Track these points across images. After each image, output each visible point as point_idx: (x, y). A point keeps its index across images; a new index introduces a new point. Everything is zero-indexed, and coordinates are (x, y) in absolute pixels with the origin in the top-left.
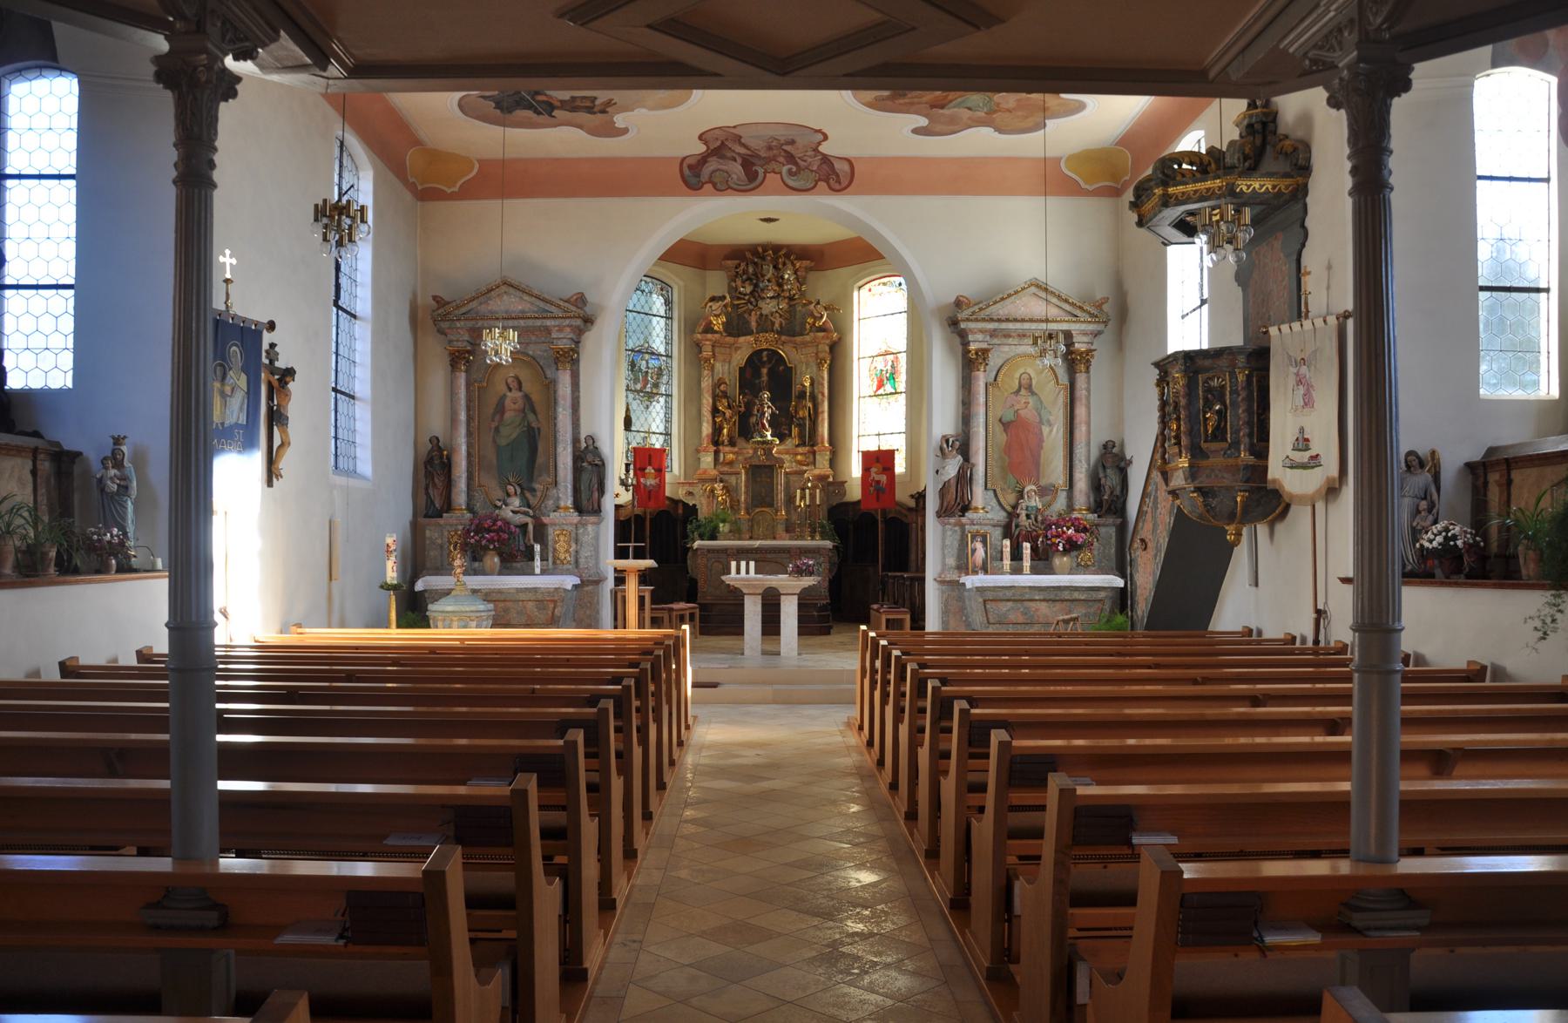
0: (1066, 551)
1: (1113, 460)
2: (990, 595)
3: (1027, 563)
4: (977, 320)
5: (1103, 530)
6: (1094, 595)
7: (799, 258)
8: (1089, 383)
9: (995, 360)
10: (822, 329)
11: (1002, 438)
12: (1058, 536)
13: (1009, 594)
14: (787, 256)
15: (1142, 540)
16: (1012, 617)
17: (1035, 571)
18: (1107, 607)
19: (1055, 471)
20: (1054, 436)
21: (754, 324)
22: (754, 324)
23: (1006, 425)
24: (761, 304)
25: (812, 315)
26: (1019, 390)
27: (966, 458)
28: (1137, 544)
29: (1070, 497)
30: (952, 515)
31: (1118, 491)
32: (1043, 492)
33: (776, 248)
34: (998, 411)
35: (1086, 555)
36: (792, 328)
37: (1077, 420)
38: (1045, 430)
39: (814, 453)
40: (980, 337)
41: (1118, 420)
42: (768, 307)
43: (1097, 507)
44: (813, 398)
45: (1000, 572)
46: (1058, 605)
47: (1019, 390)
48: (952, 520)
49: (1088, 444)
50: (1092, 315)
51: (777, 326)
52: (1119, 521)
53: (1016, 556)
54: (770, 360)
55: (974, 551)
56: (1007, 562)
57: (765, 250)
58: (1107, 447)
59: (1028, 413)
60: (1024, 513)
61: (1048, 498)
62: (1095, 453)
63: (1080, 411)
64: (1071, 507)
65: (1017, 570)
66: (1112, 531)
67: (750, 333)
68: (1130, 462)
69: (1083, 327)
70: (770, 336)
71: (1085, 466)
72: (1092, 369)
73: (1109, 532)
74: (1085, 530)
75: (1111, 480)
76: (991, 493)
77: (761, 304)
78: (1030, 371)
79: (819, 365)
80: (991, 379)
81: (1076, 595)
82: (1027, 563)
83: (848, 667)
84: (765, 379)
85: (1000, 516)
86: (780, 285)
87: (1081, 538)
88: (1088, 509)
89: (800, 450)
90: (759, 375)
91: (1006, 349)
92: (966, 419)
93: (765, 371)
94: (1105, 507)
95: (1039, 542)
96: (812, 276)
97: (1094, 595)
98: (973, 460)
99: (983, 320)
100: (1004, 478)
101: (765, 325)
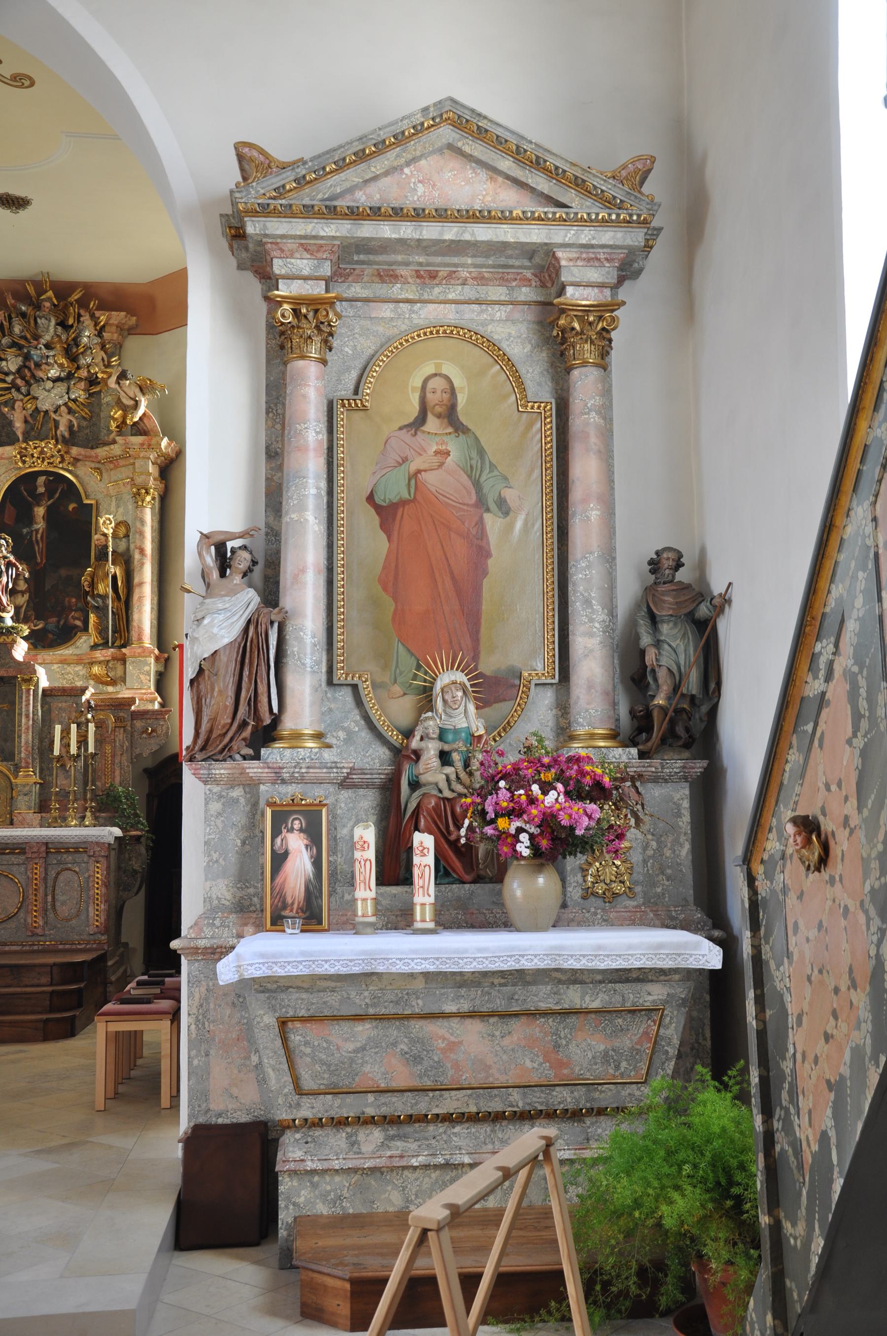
0: (541, 857)
1: (681, 603)
2: (297, 1004)
3: (425, 892)
4: (288, 212)
5: (653, 793)
6: (632, 996)
7: (104, 306)
8: (607, 393)
9: (355, 337)
10: (139, 429)
11: (370, 543)
12: (515, 812)
13: (360, 1000)
14: (83, 303)
15: (808, 826)
16: (374, 1071)
17: (451, 918)
18: (673, 1032)
19: (518, 639)
20: (515, 538)
21: (19, 426)
22: (19, 426)
23: (387, 514)
24: (37, 391)
25: (119, 404)
26: (421, 419)
27: (271, 594)
28: (784, 838)
29: (563, 707)
30: (225, 753)
31: (693, 683)
32: (491, 690)
33: (63, 290)
34: (356, 479)
35: (606, 868)
36: (87, 434)
37: (576, 494)
38: (493, 523)
39: (123, 660)
40: (303, 264)
41: (684, 485)
42: (50, 397)
43: (640, 730)
44: (126, 561)
45: (347, 923)
46: (519, 1029)
47: (421, 419)
48: (221, 770)
49: (609, 557)
50: (609, 203)
51: (63, 428)
52: (699, 766)
53: (394, 868)
54: (50, 492)
55: (280, 859)
56: (366, 892)
57: (40, 291)
58: (662, 566)
59: (446, 481)
60: (431, 750)
61: (502, 709)
62: (629, 588)
63: (585, 469)
64: (565, 732)
65: (399, 919)
66: (681, 794)
67: (11, 440)
68: (726, 601)
69: (586, 236)
70: (49, 447)
71: (601, 615)
72: (615, 356)
73: (668, 796)
74: (598, 792)
75: (673, 652)
76: (345, 696)
77: (37, 391)
78: (448, 369)
79: (137, 497)
80: (346, 388)
81: (574, 997)
82: (425, 892)
83: (163, 1100)
84: (40, 525)
85: (375, 759)
86: (73, 358)
87: (584, 816)
88: (613, 736)
89: (99, 655)
90: (30, 519)
91: (386, 311)
92: (274, 496)
93: (40, 511)
94: (658, 729)
95: (463, 839)
96: (133, 344)
97: (632, 996)
98: (287, 601)
99: (308, 212)
100: (383, 657)
101: (39, 425)
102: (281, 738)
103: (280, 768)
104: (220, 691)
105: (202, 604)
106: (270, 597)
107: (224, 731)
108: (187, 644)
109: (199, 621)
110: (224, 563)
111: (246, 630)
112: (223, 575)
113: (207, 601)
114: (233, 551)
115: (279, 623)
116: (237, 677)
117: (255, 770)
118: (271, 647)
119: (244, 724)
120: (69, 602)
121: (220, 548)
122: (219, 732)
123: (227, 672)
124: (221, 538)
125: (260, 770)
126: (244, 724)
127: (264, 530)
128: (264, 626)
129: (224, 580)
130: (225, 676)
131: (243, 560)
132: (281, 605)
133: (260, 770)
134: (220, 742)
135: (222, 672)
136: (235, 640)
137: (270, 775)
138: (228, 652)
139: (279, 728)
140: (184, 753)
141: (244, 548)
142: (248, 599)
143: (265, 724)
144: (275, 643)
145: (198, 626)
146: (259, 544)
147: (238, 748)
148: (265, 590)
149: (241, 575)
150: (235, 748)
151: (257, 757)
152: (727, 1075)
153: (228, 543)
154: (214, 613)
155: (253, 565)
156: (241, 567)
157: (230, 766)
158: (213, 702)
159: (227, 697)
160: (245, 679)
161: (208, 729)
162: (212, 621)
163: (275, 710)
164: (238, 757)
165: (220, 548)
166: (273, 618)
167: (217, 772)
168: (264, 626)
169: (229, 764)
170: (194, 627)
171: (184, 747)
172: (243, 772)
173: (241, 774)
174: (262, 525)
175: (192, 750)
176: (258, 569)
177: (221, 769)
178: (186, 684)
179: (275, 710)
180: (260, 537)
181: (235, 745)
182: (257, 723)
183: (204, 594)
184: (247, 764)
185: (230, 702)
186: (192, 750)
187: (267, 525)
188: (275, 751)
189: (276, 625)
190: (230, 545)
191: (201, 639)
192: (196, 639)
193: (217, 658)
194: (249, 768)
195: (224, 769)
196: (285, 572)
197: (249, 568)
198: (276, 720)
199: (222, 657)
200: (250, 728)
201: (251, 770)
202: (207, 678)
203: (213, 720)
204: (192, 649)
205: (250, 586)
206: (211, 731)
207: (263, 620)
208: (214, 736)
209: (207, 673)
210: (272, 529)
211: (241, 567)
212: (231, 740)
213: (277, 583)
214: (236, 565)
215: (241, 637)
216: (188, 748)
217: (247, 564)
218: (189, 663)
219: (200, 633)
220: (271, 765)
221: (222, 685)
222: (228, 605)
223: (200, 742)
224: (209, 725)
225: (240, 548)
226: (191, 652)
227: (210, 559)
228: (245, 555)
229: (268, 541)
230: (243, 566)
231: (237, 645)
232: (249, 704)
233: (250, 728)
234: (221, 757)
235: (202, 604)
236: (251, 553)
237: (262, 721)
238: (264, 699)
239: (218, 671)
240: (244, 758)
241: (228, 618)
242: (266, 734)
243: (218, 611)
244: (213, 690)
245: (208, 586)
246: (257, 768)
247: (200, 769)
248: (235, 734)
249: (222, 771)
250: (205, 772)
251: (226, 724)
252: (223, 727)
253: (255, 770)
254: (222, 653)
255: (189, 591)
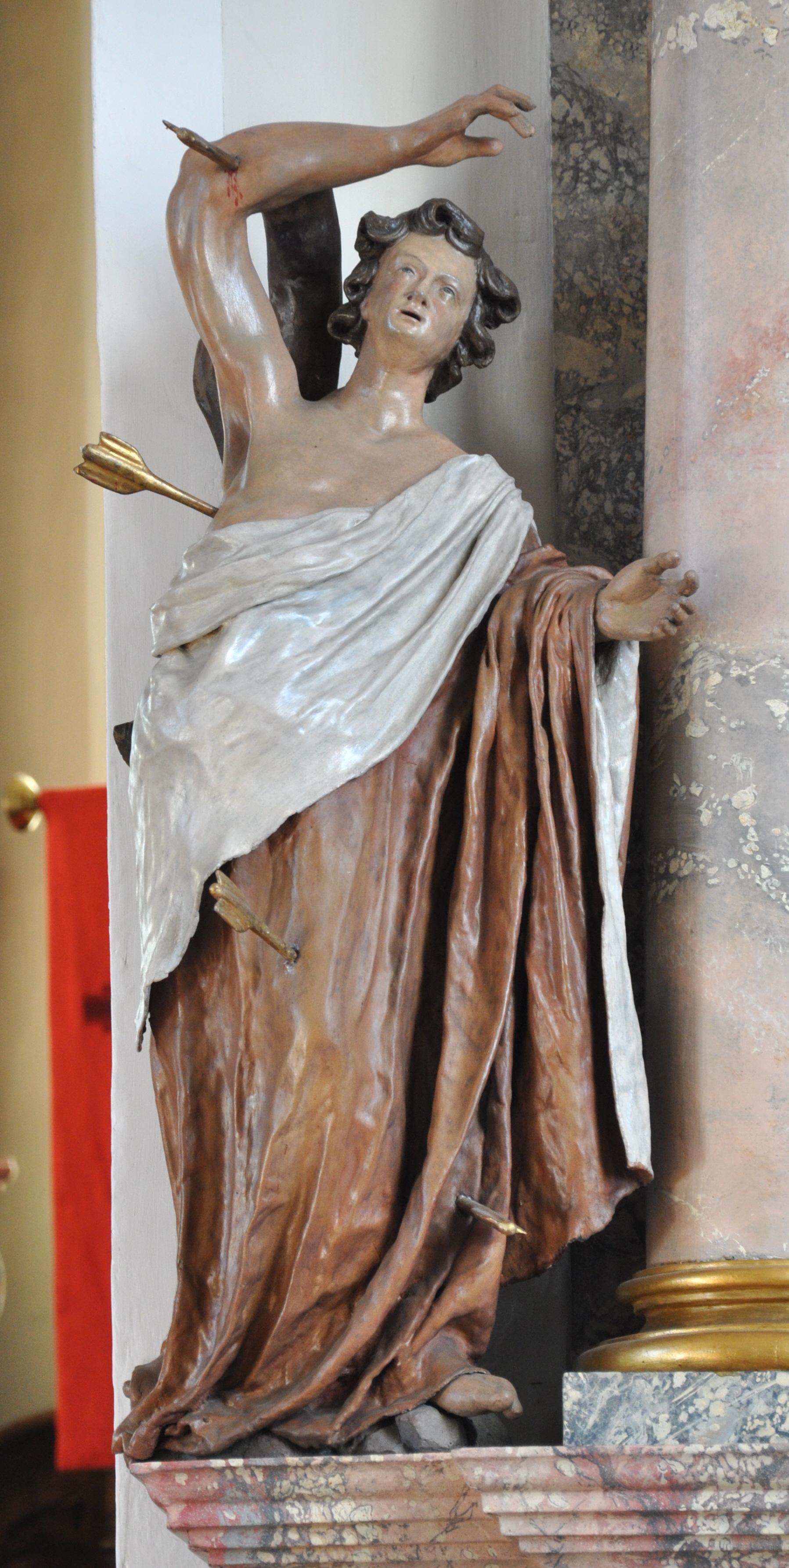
30: (358, 1407)
102: (674, 1314)
103: (675, 1486)
104: (322, 1050)
105: (206, 552)
106: (587, 502)
107: (350, 1274)
108: (124, 787)
109: (193, 650)
110: (322, 314)
111: (458, 697)
112: (317, 381)
113: (238, 534)
114: (374, 238)
115: (646, 649)
116: (412, 969)
117: (534, 1501)
118: (604, 787)
119: (461, 1234)
120: (189, 564)
121: (300, 223)
122: (322, 1283)
123: (356, 937)
124: (307, 162)
125: (559, 1502)
126: (461, 1234)
127: (544, 107)
128: (559, 671)
129: (326, 413)
130: (346, 962)
131: (433, 290)
132: (655, 543)
133: (559, 1502)
134: (330, 1342)
135: (329, 939)
136: (401, 754)
137: (616, 1527)
138: (358, 823)
139: (659, 1256)
140: (122, 1408)
141: (436, 218)
142: (445, 521)
143: (578, 1231)
144: (625, 765)
145: (189, 679)
146: (519, 190)
147: (432, 1375)
148: (557, 463)
149: (421, 382)
150: (415, 1371)
151: (539, 1423)
152: (409, 1501)
153: (341, 195)
154: (273, 604)
155: (492, 321)
156: (422, 330)
157: (387, 1479)
158: (281, 1114)
159: (361, 1082)
160: (462, 973)
161: (256, 1268)
162: (268, 648)
163: (638, 1151)
164: (429, 1424)
165: (300, 223)
166: (612, 618)
167: (317, 1513)
168: (559, 671)
169: (380, 1466)
170: (167, 684)
171: (121, 1373)
172: (462, 1513)
173: (453, 1522)
174: (533, 80)
175: (169, 1391)
176: (517, 343)
177: (338, 1495)
178: (128, 1011)
179: (638, 1151)
180: (525, 154)
181: (412, 1355)
182: (536, 1227)
183: (215, 497)
184: (482, 1463)
185: (378, 1109)
186: (169, 1391)
187: (565, 79)
188: (641, 1386)
189: (628, 663)
190: (351, 205)
191: (205, 755)
192: (181, 753)
193: (302, 857)
194: (500, 1488)
195: (357, 1495)
196: (675, 353)
197: (467, 335)
198: (645, 1207)
199: (328, 854)
200: (494, 1254)
201: (510, 1502)
202: (244, 975)
203: (287, 1217)
204: (157, 810)
205: (474, 439)
206: (272, 1279)
207: (559, 637)
208: (293, 1304)
209: (243, 944)
210: (593, 103)
211: (422, 330)
212: (392, 1325)
213: (630, 419)
214: (396, 323)
215: (429, 737)
216: (143, 1378)
217: (458, 316)
218: (142, 890)
219: (201, 720)
220: (621, 1470)
221: (329, 1013)
222: (351, 557)
223: (214, 1343)
224: (262, 1244)
225: (412, 220)
226: (153, 828)
227: (244, 297)
228: (442, 262)
229: (570, 175)
230: (433, 327)
231: (409, 783)
232: (486, 1119)
233: (494, 1254)
234: (332, 1429)
235: (206, 552)
236: (476, 250)
237: (564, 1216)
238: (572, 1090)
239: (307, 933)
240: (467, 1429)
241: (357, 631)
242: (591, 1293)
243: (301, 592)
244: (280, 1038)
245: (235, 446)
246: (546, 1488)
247: (217, 1498)
248: (409, 1292)
249: (344, 1511)
250: (250, 1514)
251: (364, 1234)
252: (344, 1252)
253: (534, 1501)
254: (327, 830)
255: (126, 483)
